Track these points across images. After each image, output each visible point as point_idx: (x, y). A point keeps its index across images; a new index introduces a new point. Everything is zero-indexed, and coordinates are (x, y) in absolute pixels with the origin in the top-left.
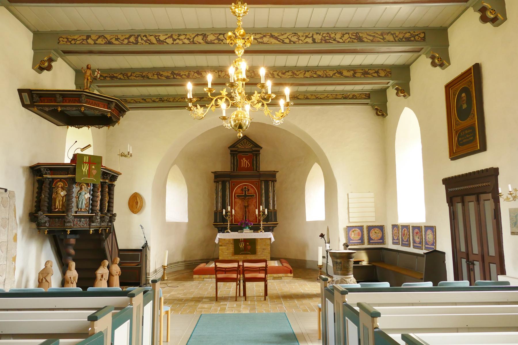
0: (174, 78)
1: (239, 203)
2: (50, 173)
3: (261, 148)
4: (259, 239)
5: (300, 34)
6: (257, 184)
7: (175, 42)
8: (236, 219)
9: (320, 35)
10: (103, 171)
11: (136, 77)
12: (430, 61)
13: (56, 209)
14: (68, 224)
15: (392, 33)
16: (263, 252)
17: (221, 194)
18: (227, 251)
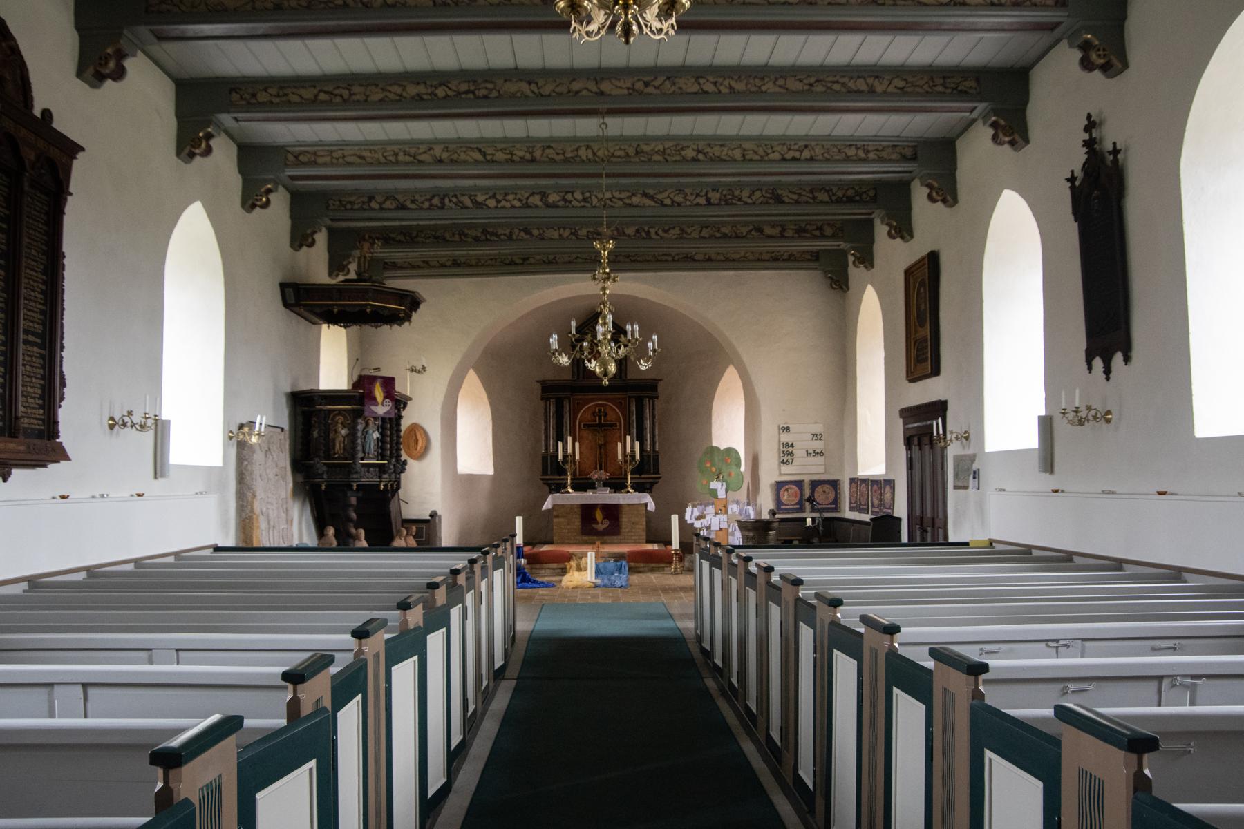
0: (487, 240)
5: (687, 190)
6: (621, 403)
7: (499, 206)
9: (717, 192)
11: (426, 239)
12: (1078, 55)
13: (335, 454)
14: (355, 476)
15: (827, 188)
18: (569, 527)
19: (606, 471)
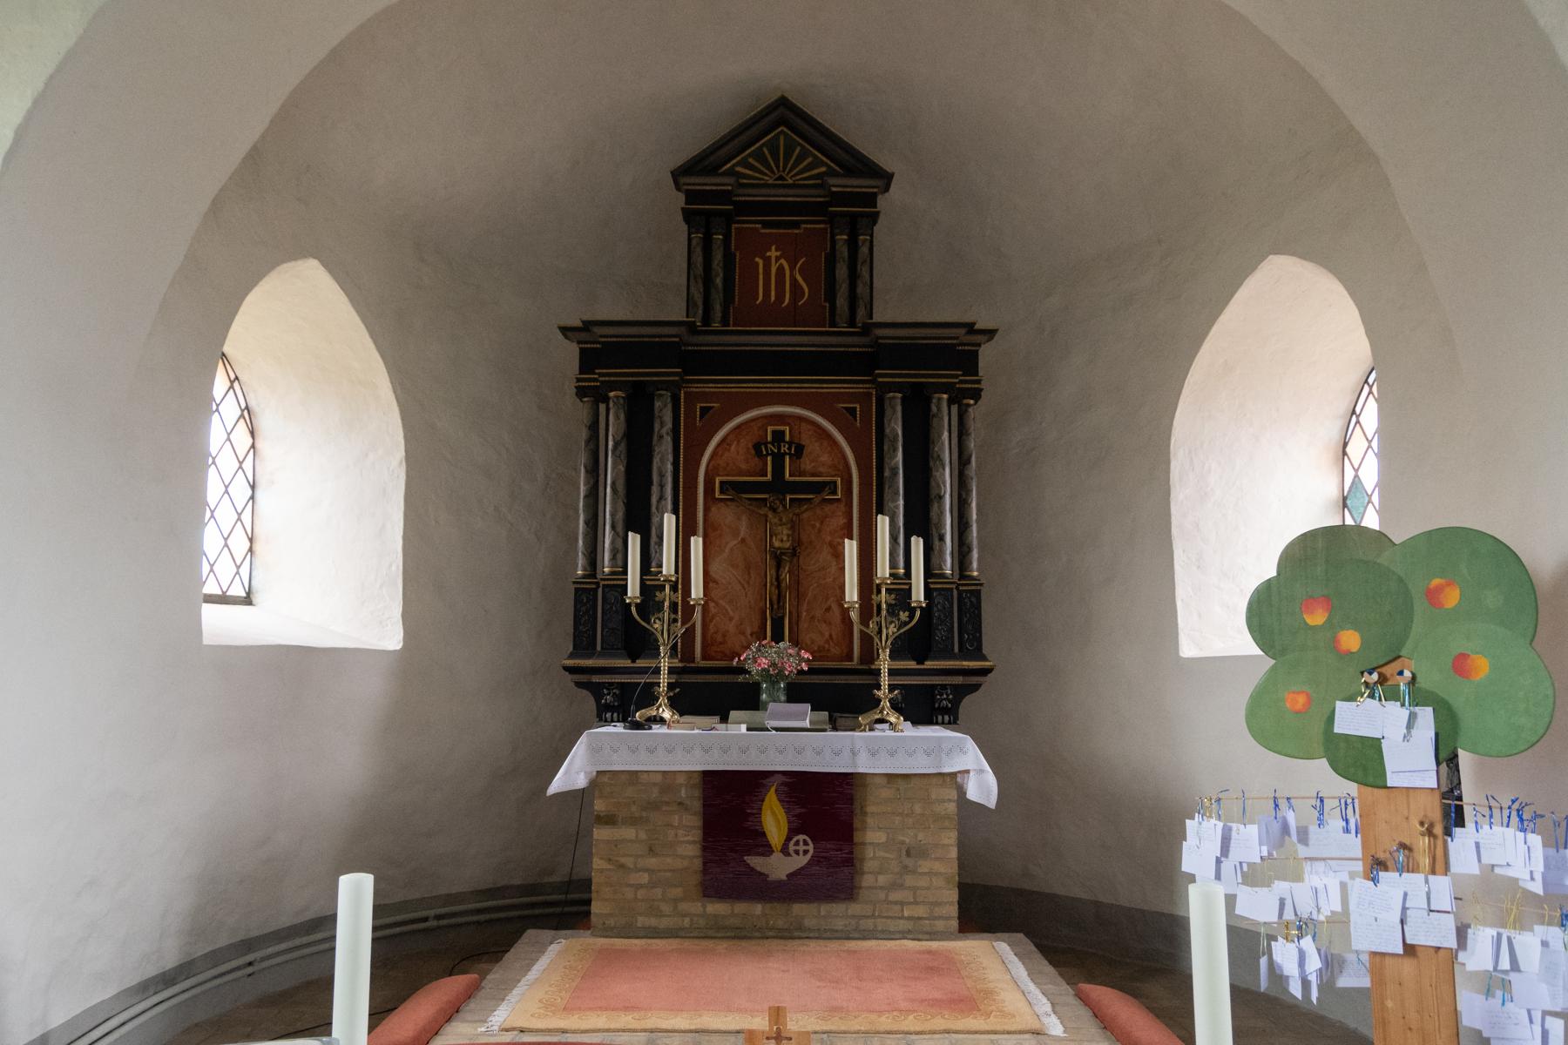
1: (736, 533)
3: (887, 178)
4: (878, 780)
6: (852, 411)
8: (719, 638)
16: (906, 869)
17: (622, 468)
18: (652, 862)
19: (795, 642)
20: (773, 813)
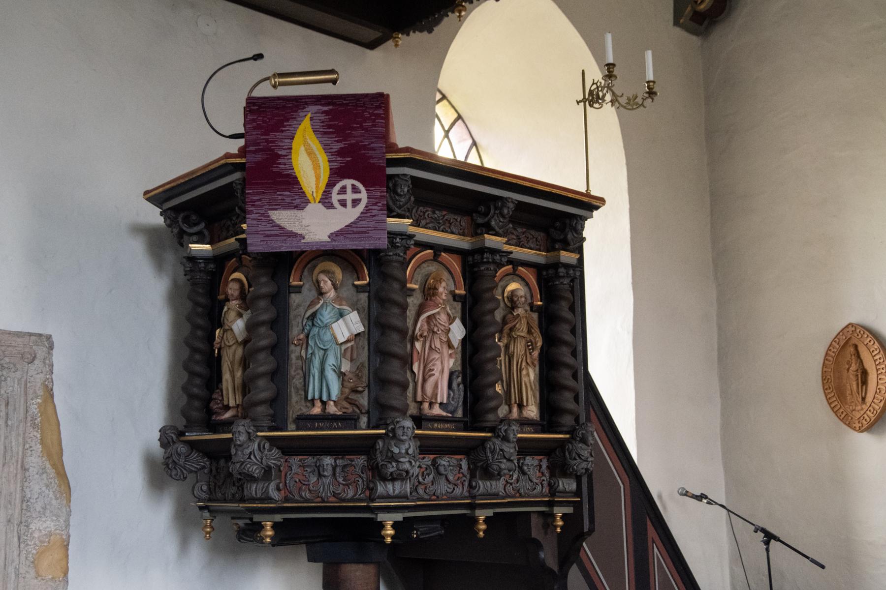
2: (206, 233)
10: (520, 202)
20: (310, 153)
